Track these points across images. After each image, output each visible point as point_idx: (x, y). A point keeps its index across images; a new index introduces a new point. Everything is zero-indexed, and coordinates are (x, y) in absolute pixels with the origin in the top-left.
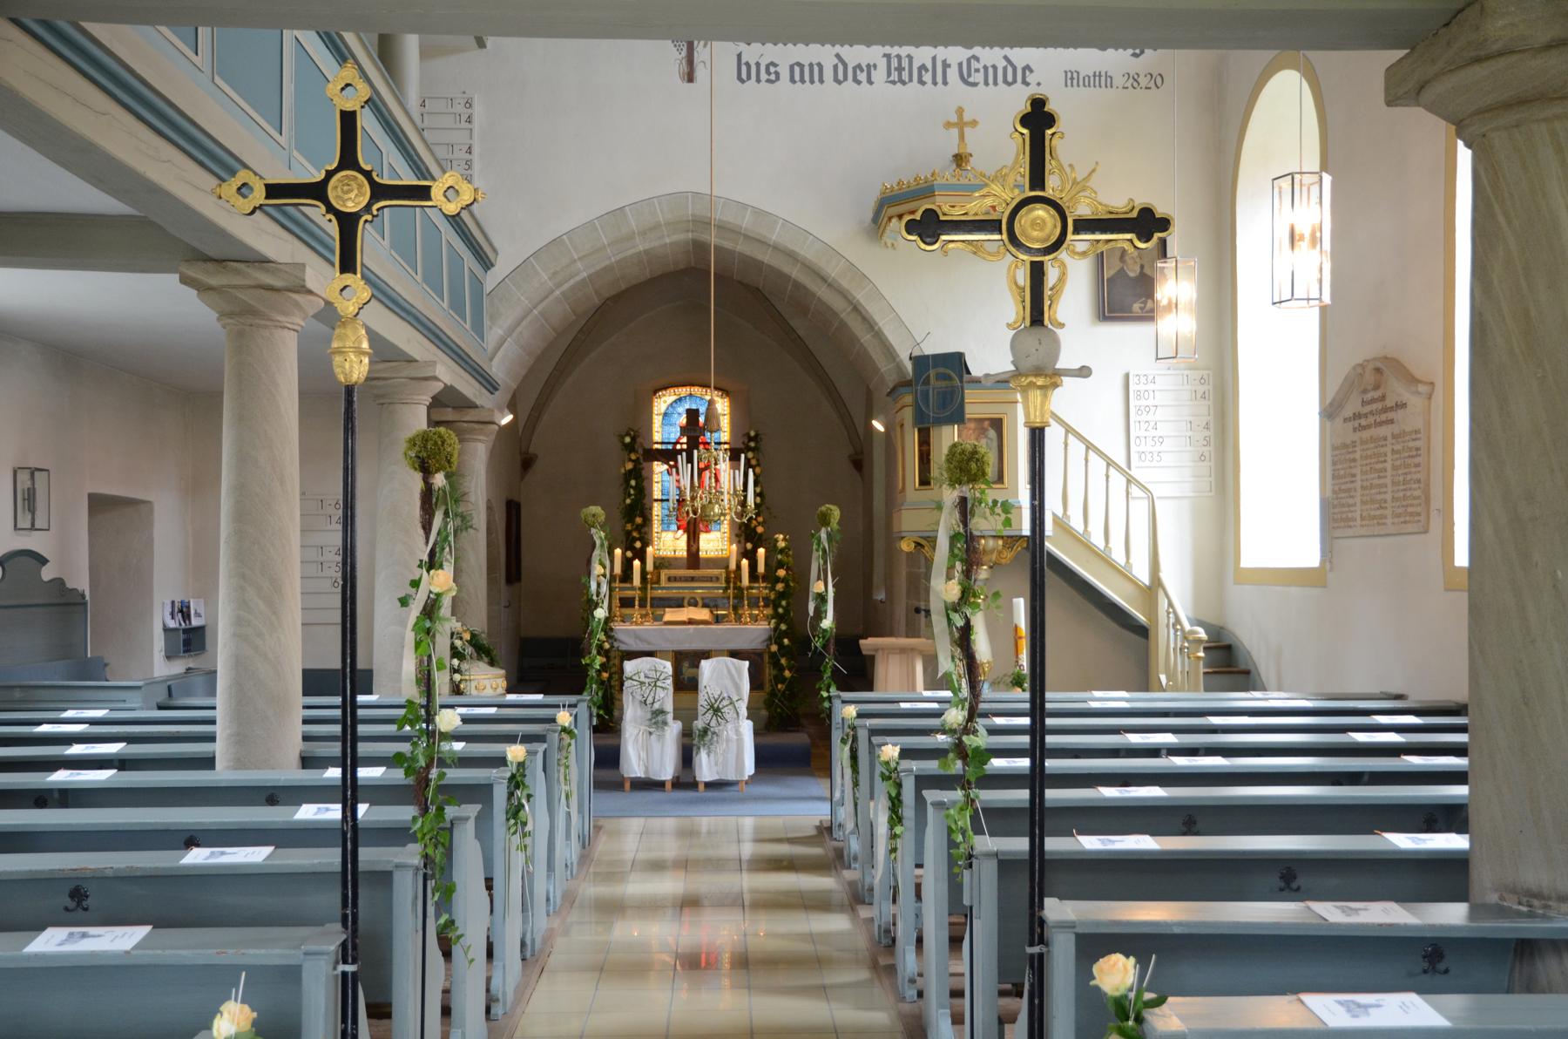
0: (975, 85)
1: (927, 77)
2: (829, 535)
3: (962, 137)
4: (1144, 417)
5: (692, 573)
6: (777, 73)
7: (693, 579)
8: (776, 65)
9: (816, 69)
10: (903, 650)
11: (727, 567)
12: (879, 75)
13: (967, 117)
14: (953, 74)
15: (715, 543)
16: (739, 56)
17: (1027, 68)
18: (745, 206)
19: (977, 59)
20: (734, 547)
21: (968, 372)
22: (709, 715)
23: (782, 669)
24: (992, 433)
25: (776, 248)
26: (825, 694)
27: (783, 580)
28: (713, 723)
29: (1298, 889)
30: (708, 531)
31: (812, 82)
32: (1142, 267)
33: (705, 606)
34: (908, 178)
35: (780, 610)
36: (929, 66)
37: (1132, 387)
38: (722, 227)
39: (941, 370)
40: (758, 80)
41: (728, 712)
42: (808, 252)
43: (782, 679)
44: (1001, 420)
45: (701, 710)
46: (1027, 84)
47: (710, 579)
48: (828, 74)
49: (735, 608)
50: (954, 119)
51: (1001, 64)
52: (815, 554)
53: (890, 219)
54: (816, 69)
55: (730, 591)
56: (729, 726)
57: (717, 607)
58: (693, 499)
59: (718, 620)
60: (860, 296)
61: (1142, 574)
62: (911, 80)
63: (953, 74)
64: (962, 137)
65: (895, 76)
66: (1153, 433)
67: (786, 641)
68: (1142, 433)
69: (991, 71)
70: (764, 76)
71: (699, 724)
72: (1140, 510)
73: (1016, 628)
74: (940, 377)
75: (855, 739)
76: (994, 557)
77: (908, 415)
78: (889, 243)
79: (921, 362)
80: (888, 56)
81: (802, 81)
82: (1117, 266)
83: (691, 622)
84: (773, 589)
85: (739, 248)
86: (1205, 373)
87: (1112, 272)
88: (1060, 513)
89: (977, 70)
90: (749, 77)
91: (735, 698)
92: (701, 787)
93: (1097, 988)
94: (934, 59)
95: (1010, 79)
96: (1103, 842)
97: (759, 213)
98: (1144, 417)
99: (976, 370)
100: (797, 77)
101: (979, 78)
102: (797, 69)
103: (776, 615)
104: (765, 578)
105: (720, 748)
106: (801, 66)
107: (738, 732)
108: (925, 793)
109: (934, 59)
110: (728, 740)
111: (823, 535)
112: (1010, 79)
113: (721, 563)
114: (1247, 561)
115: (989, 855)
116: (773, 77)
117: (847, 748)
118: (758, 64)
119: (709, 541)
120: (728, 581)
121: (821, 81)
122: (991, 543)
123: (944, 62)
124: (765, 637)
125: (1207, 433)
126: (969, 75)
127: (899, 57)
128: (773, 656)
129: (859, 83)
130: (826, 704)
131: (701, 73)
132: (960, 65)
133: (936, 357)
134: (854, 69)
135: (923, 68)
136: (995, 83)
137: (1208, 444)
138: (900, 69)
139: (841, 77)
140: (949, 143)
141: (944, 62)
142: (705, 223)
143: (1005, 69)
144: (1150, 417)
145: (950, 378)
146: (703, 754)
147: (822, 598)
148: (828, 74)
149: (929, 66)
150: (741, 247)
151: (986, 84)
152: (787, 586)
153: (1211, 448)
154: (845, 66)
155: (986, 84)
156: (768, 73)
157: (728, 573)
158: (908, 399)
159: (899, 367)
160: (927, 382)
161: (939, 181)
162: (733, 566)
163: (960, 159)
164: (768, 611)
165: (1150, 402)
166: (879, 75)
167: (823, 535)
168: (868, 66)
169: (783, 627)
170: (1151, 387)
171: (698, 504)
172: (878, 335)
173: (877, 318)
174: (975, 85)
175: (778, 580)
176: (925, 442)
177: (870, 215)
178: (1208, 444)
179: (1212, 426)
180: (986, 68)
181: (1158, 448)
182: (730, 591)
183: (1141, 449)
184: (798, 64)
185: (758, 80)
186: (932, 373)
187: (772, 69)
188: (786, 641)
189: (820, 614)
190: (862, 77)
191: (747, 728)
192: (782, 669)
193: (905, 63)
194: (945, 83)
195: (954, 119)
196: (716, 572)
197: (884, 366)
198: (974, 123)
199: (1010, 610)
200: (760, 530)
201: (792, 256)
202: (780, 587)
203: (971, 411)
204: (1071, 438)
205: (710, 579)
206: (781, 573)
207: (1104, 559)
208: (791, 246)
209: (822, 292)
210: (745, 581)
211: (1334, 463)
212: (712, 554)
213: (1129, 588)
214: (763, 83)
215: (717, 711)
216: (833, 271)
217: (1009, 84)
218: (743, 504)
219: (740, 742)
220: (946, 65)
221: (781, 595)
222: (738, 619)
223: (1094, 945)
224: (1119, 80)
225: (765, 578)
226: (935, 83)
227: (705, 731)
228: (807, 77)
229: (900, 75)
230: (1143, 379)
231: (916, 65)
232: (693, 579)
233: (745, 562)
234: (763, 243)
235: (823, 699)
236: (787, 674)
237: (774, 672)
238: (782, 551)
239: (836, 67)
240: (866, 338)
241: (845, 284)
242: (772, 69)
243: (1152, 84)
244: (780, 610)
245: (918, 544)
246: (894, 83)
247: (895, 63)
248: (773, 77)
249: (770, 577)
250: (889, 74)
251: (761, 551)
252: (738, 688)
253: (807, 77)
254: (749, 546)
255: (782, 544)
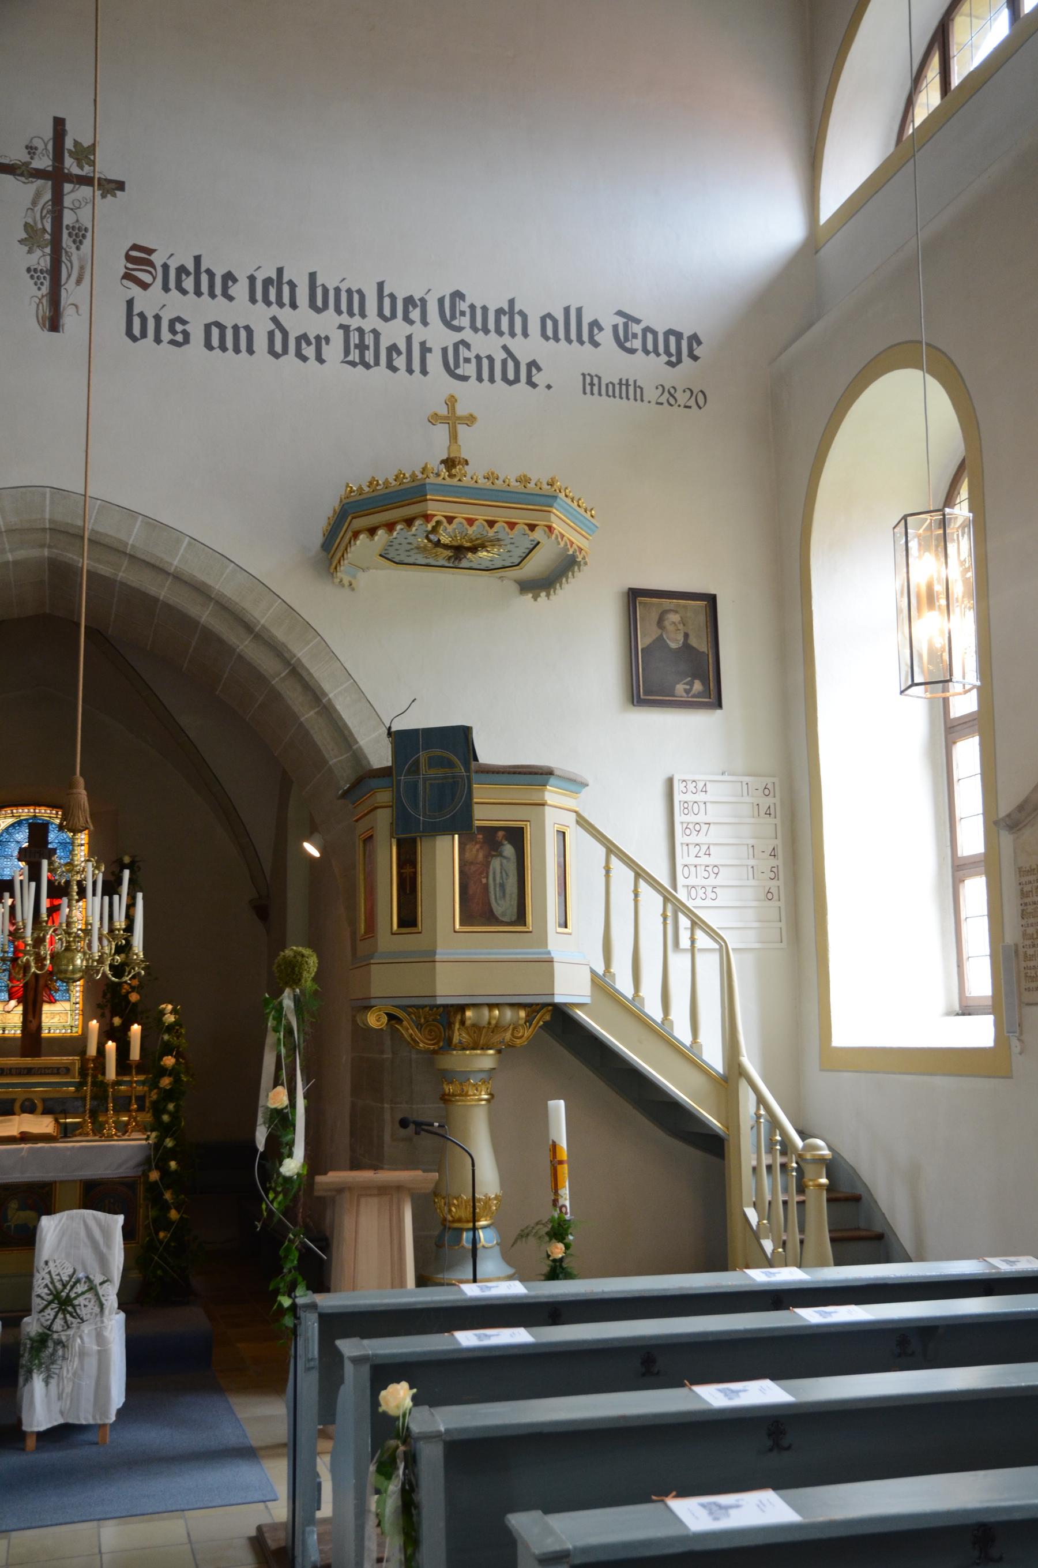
0: (464, 378)
1: (400, 362)
2: (297, 1001)
3: (454, 436)
4: (693, 839)
5: (28, 1061)
6: (186, 334)
7: (29, 1071)
8: (184, 322)
9: (243, 334)
10: (383, 1190)
11: (83, 1052)
12: (334, 351)
13: (461, 410)
14: (434, 361)
15: (61, 1017)
16: (130, 303)
17: (533, 365)
18: (133, 514)
19: (467, 346)
20: (94, 1024)
21: (476, 759)
22: (50, 1313)
23: (165, 1207)
24: (508, 850)
25: (178, 578)
26: (286, 1302)
27: (172, 1072)
28: (58, 1325)
29: (658, 1373)
30: (52, 1001)
31: (237, 350)
32: (686, 636)
33: (46, 1112)
34: (386, 474)
35: (166, 1118)
36: (403, 347)
37: (677, 797)
38: (99, 544)
39: (437, 752)
40: (158, 340)
41: (85, 1305)
42: (225, 586)
43: (167, 1224)
44: (521, 830)
45: (37, 1303)
46: (534, 385)
47: (56, 1071)
48: (261, 342)
49: (94, 1114)
50: (443, 411)
51: (499, 356)
52: (271, 1038)
53: (356, 535)
54: (243, 334)
55: (87, 1089)
56: (87, 1329)
57: (66, 1113)
58: (38, 942)
59: (66, 1132)
60: (302, 653)
61: (714, 1057)
62: (377, 363)
63: (434, 361)
64: (454, 436)
65: (355, 355)
66: (705, 860)
67: (173, 1164)
68: (692, 860)
69: (485, 363)
70: (166, 336)
71: (32, 1326)
72: (709, 968)
73: (554, 1146)
74: (432, 762)
75: (412, 1460)
76: (508, 1036)
77: (383, 820)
78: (346, 580)
79: (404, 741)
80: (345, 328)
81: (223, 348)
82: (654, 633)
83: (24, 1138)
84: (154, 1084)
85: (121, 575)
86: (769, 780)
87: (648, 641)
88: (600, 969)
89: (467, 360)
90: (144, 334)
91: (98, 1279)
92: (31, 1443)
93: (385, 1413)
94: (409, 339)
95: (511, 376)
96: (479, 1337)
97: (153, 525)
98: (693, 839)
99: (489, 751)
100: (215, 341)
101: (470, 370)
102: (215, 331)
103: (157, 1125)
104: (140, 1068)
105: (68, 1369)
106: (222, 328)
107: (100, 1337)
108: (340, 1343)
109: (409, 339)
110: (82, 1354)
111: (287, 1002)
112: (511, 376)
113: (74, 1045)
114: (846, 1033)
115: (357, 1361)
116: (179, 338)
117: (394, 1487)
118: (158, 318)
119: (53, 1014)
120: (83, 1072)
121: (250, 351)
122: (509, 1014)
123: (423, 344)
124: (140, 1157)
125: (773, 862)
126: (457, 365)
127: (360, 331)
128: (152, 1187)
129: (304, 359)
130: (288, 1321)
131: (69, 319)
132: (445, 350)
133: (428, 732)
134: (298, 340)
135: (393, 349)
136: (492, 380)
137: (776, 877)
138: (362, 347)
139: (278, 348)
140: (434, 445)
141: (423, 344)
142: (76, 536)
143: (504, 362)
144: (700, 839)
145: (451, 765)
146: (38, 1382)
147: (282, 1120)
148: (261, 342)
149: (403, 347)
150: (126, 575)
151: (480, 379)
152: (177, 1080)
153: (780, 883)
154: (285, 334)
155: (480, 379)
156: (172, 330)
157: (84, 1061)
158: (384, 796)
159: (357, 757)
160: (415, 769)
161: (432, 479)
162: (92, 1050)
163: (450, 463)
164: (146, 1117)
165: (701, 818)
166: (334, 351)
167: (287, 1002)
168: (318, 338)
169: (169, 1143)
170: (700, 797)
171: (46, 950)
172: (328, 712)
173: (326, 686)
174: (464, 378)
175: (163, 1072)
176: (408, 861)
177: (318, 539)
178: (776, 877)
179: (780, 852)
180: (478, 358)
181: (712, 881)
182: (87, 1089)
183: (691, 881)
184: (218, 324)
185: (158, 340)
186: (423, 756)
187: (179, 327)
188: (173, 1164)
189: (278, 1149)
190: (309, 351)
191: (115, 1325)
192: (165, 1207)
193: (369, 340)
194: (424, 372)
195: (443, 411)
196: (66, 1059)
197: (335, 758)
198: (470, 420)
199: (544, 1117)
200: (134, 997)
201: (201, 591)
202: (166, 1082)
203: (483, 815)
204: (615, 862)
205: (56, 1071)
206: (169, 1061)
207: (660, 1034)
208: (202, 576)
209: (245, 646)
210: (111, 1074)
211: (1023, 894)
212: (57, 1033)
213: (697, 1080)
214: (164, 345)
215: (64, 1303)
216: (262, 615)
217: (510, 383)
218: (124, 949)
219: (103, 1356)
220: (425, 349)
221: (168, 1095)
222: (98, 1130)
223: (384, 1373)
224: (651, 394)
225: (140, 1068)
226: (410, 371)
227: (42, 1340)
228: (229, 343)
229: (362, 356)
230: (691, 787)
231: (384, 344)
232: (29, 1071)
233: (111, 1045)
234: (158, 569)
235: (282, 1311)
236: (174, 1215)
237: (152, 1213)
238: (170, 1028)
239: (271, 335)
240: (308, 715)
241: (280, 634)
242: (179, 327)
243: (692, 403)
244: (166, 1118)
245: (391, 1017)
246: (353, 364)
247: (355, 338)
248: (179, 338)
249: (150, 1065)
250: (347, 352)
251: (136, 1028)
252: (103, 1262)
253: (229, 343)
254: (117, 1021)
255: (170, 1019)
